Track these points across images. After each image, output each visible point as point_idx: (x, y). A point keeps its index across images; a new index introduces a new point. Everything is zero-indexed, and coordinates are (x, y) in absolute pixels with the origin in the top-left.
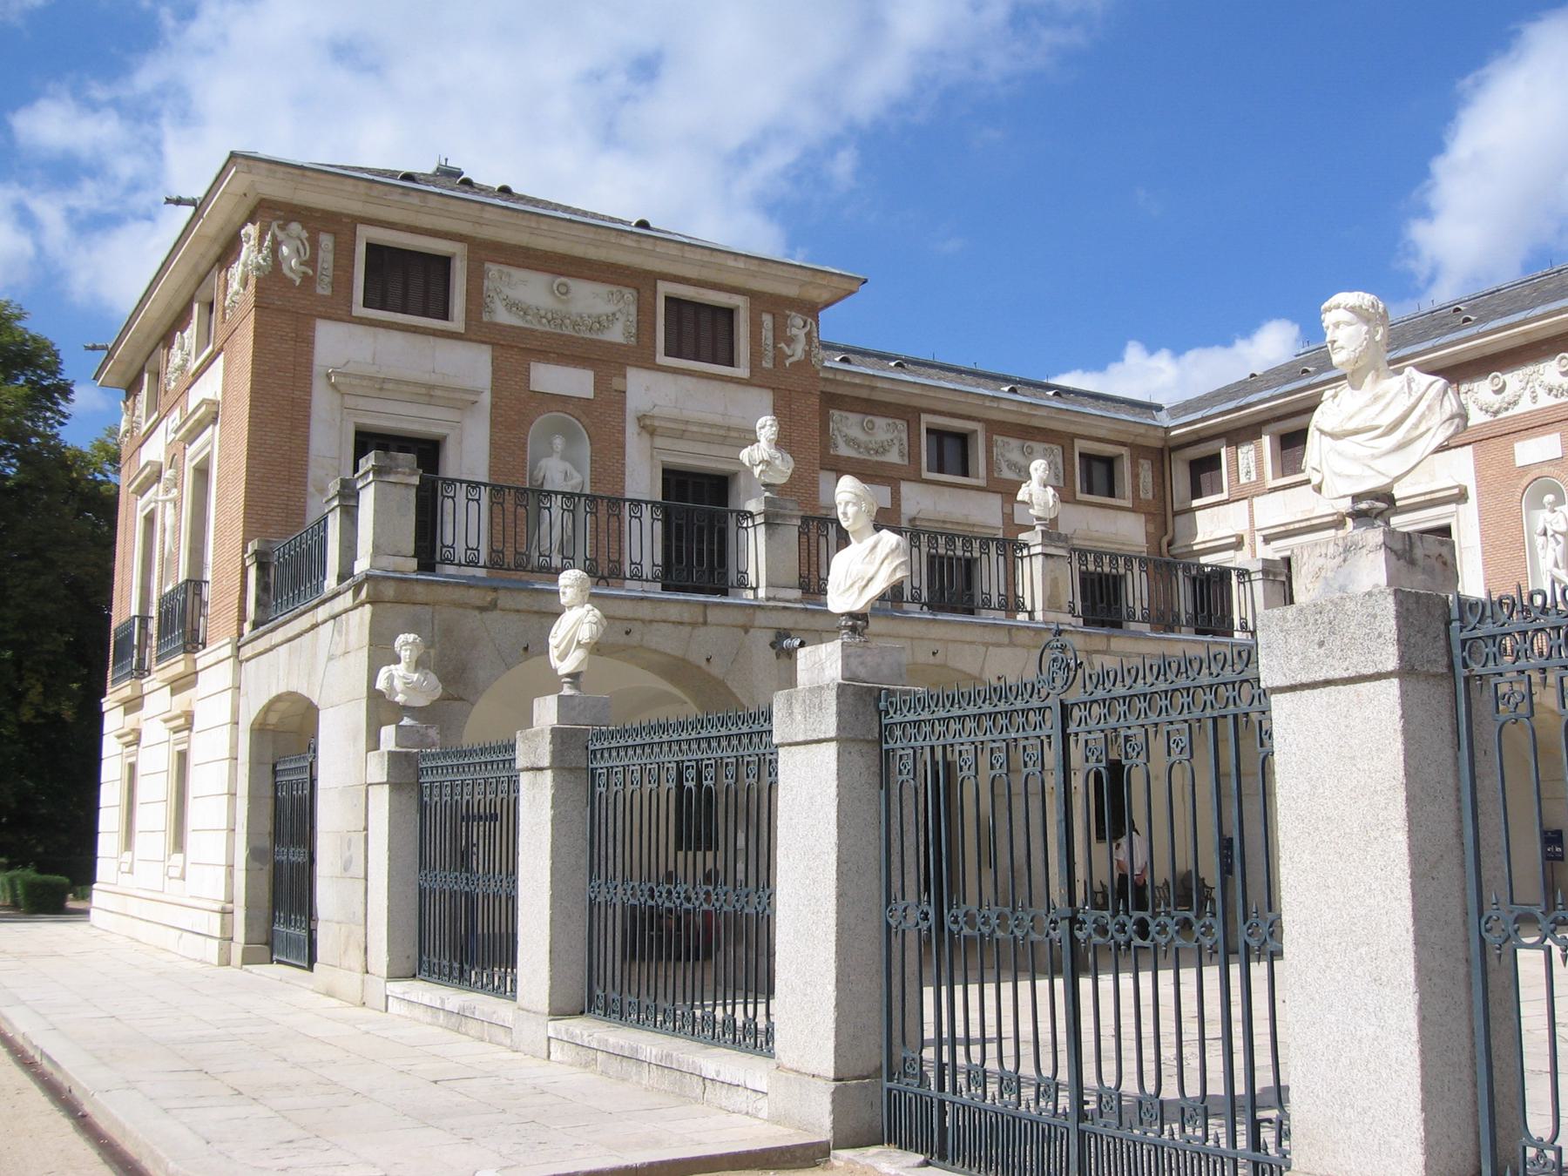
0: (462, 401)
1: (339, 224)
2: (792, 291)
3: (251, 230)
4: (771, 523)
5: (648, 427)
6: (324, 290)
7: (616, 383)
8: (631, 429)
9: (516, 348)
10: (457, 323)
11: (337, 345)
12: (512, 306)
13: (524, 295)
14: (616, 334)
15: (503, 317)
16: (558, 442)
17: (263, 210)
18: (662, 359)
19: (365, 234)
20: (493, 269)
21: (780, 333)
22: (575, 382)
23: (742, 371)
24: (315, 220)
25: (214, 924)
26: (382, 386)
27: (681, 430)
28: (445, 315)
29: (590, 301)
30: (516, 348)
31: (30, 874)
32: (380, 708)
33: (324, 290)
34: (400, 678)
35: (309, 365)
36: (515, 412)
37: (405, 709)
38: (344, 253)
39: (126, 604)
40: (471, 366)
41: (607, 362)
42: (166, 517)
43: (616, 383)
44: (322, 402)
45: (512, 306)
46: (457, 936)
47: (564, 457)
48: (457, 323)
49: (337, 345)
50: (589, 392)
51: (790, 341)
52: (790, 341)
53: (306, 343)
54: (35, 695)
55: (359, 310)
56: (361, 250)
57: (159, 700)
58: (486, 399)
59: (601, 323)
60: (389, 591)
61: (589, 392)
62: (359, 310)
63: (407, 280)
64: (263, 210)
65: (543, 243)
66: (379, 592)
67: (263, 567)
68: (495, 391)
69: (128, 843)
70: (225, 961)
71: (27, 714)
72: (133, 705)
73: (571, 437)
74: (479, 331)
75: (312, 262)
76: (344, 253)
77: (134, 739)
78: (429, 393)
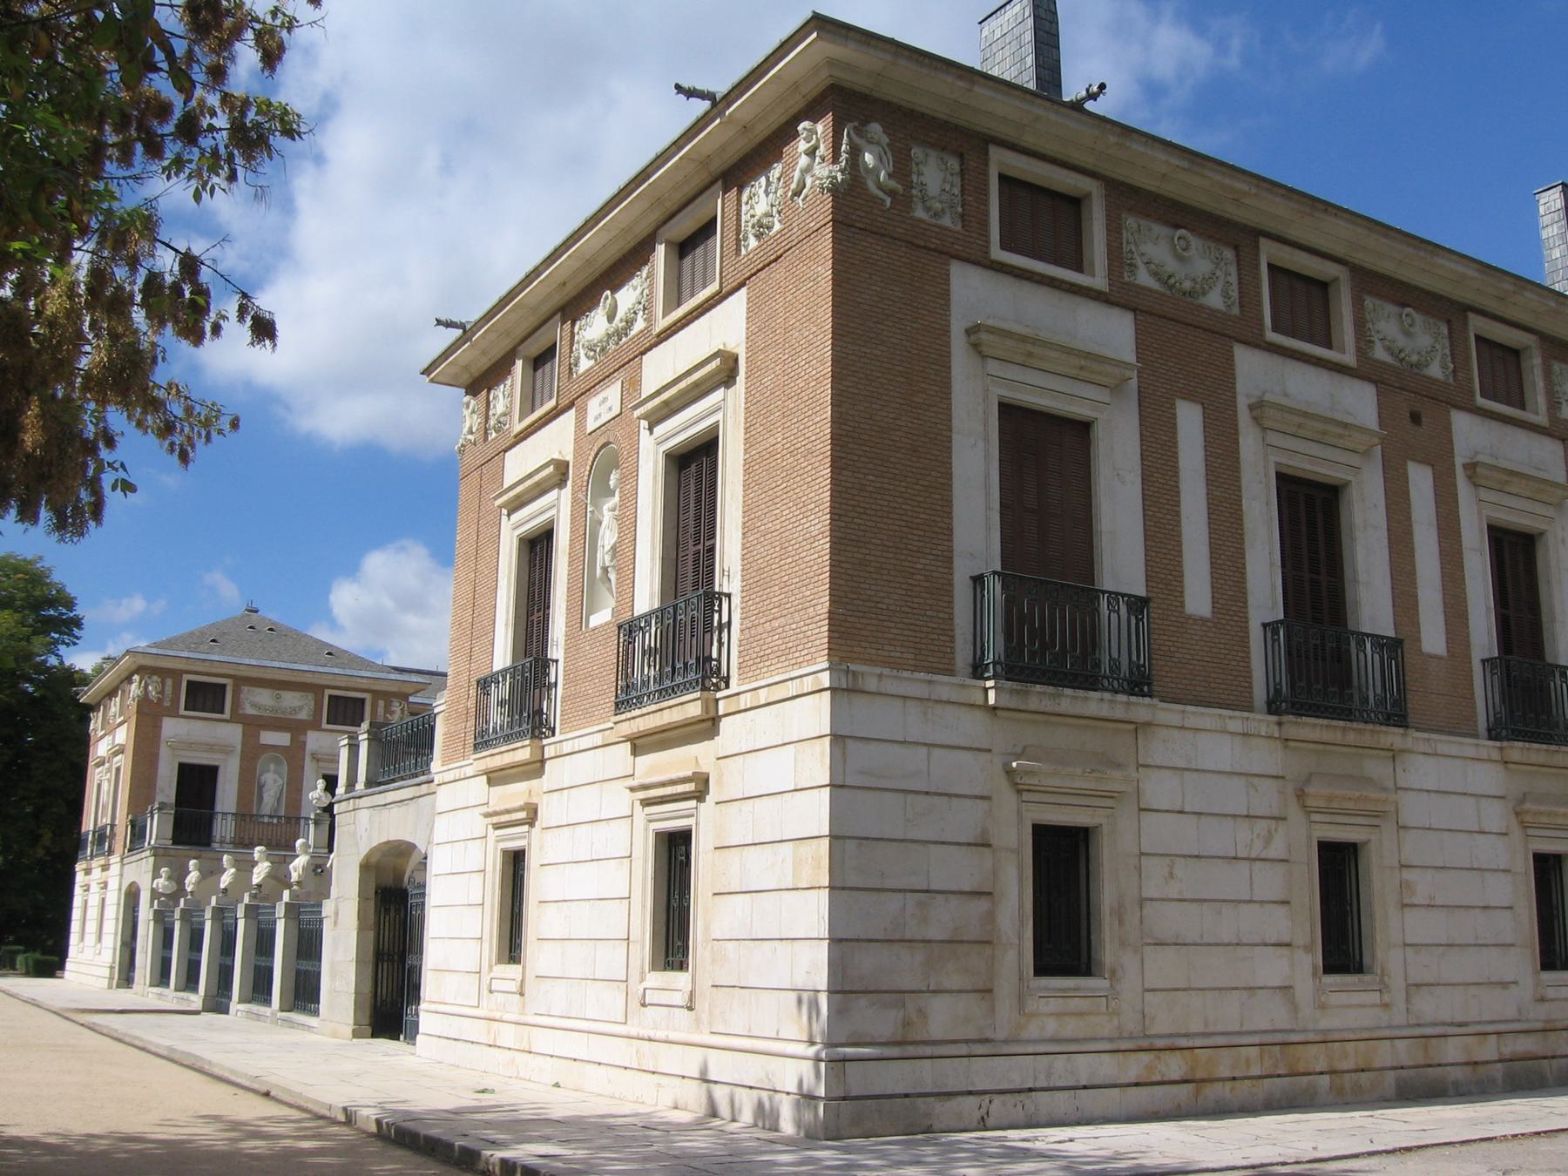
0: (226, 750)
1: (176, 674)
2: (394, 689)
3: (136, 677)
4: (316, 823)
5: (316, 758)
6: (167, 704)
7: (301, 738)
8: (308, 759)
9: (253, 725)
10: (227, 715)
11: (172, 728)
12: (253, 705)
13: (259, 700)
14: (303, 715)
15: (249, 710)
16: (272, 767)
17: (140, 670)
18: (325, 726)
19: (186, 677)
20: (245, 689)
21: (388, 710)
22: (282, 739)
23: (1098, 279)
24: (163, 673)
25: (107, 972)
26: (190, 745)
27: (1029, 349)
28: (222, 712)
29: (291, 699)
30: (253, 725)
31: (38, 955)
32: (155, 894)
33: (167, 704)
34: (161, 883)
35: (159, 737)
36: (252, 754)
37: (163, 895)
38: (177, 687)
39: (88, 825)
40: (233, 734)
41: (297, 728)
42: (105, 786)
43: (301, 738)
44: (164, 752)
45: (253, 705)
46: (161, 976)
47: (276, 772)
48: (227, 715)
49: (172, 728)
50: (288, 743)
51: (392, 713)
52: (392, 713)
53: (157, 727)
54: (47, 838)
55: (182, 711)
56: (184, 685)
57: (97, 873)
58: (239, 748)
59: (295, 710)
60: (161, 852)
61: (288, 743)
62: (182, 711)
63: (205, 696)
64: (140, 670)
65: (269, 676)
66: (157, 852)
67: (133, 827)
68: (243, 744)
69: (82, 939)
70: (110, 987)
71: (40, 853)
72: (88, 872)
73: (278, 762)
74: (237, 717)
75: (162, 692)
76: (177, 687)
77: (87, 888)
78: (211, 747)
